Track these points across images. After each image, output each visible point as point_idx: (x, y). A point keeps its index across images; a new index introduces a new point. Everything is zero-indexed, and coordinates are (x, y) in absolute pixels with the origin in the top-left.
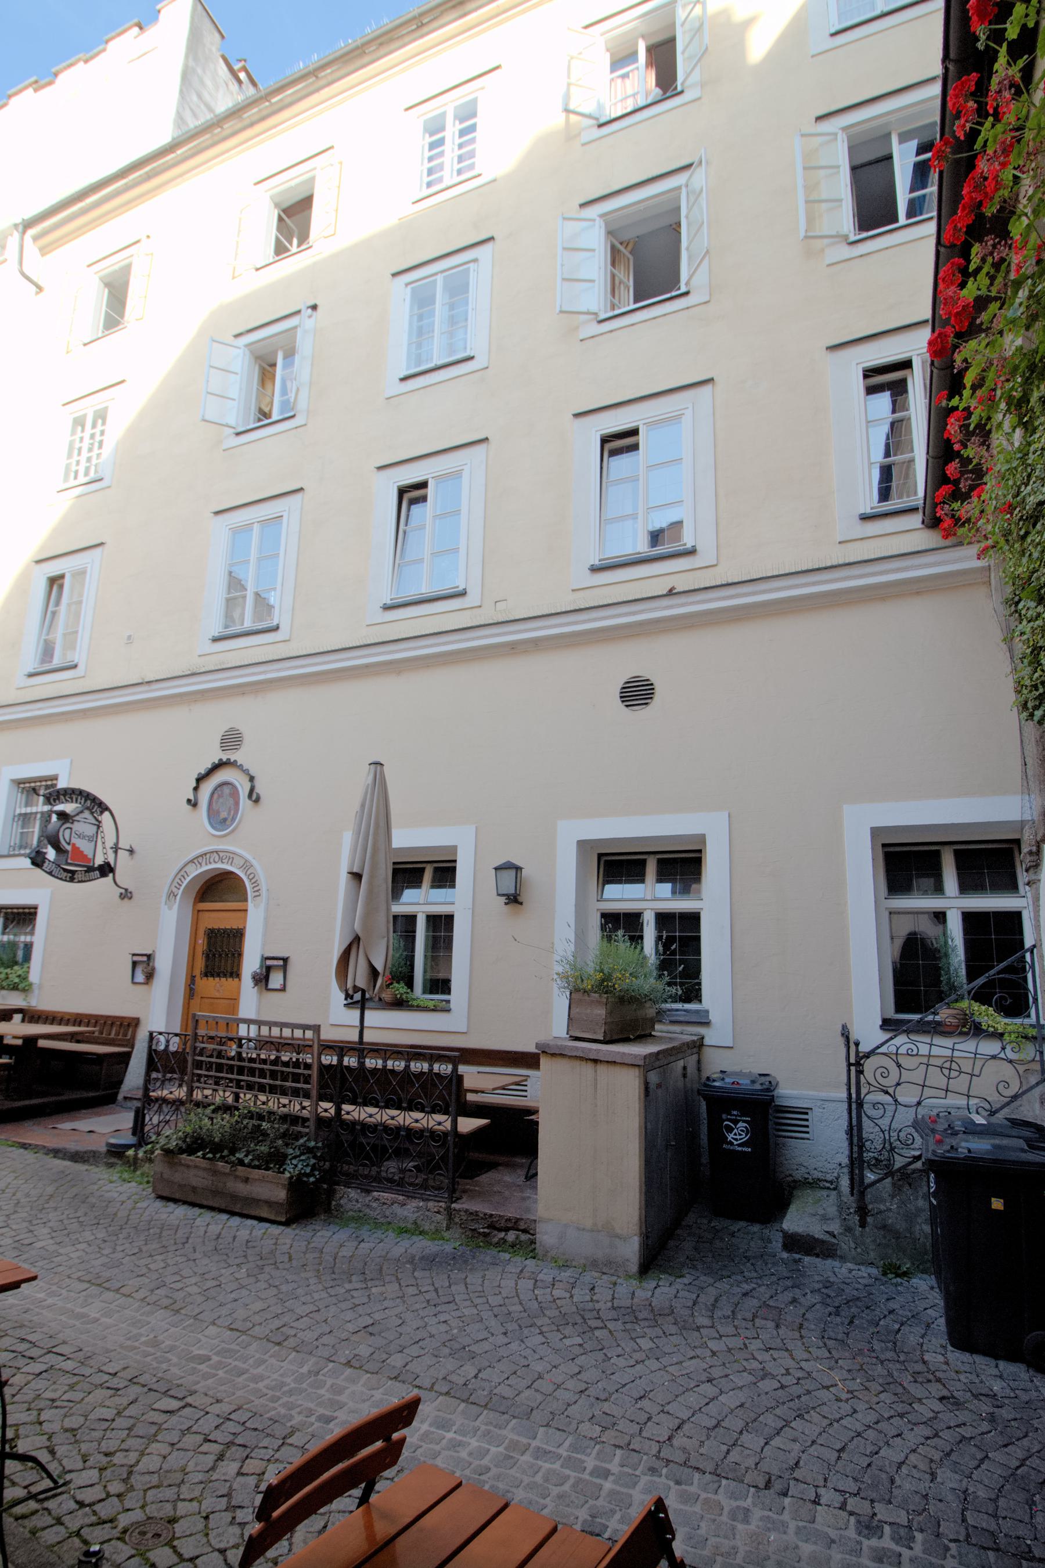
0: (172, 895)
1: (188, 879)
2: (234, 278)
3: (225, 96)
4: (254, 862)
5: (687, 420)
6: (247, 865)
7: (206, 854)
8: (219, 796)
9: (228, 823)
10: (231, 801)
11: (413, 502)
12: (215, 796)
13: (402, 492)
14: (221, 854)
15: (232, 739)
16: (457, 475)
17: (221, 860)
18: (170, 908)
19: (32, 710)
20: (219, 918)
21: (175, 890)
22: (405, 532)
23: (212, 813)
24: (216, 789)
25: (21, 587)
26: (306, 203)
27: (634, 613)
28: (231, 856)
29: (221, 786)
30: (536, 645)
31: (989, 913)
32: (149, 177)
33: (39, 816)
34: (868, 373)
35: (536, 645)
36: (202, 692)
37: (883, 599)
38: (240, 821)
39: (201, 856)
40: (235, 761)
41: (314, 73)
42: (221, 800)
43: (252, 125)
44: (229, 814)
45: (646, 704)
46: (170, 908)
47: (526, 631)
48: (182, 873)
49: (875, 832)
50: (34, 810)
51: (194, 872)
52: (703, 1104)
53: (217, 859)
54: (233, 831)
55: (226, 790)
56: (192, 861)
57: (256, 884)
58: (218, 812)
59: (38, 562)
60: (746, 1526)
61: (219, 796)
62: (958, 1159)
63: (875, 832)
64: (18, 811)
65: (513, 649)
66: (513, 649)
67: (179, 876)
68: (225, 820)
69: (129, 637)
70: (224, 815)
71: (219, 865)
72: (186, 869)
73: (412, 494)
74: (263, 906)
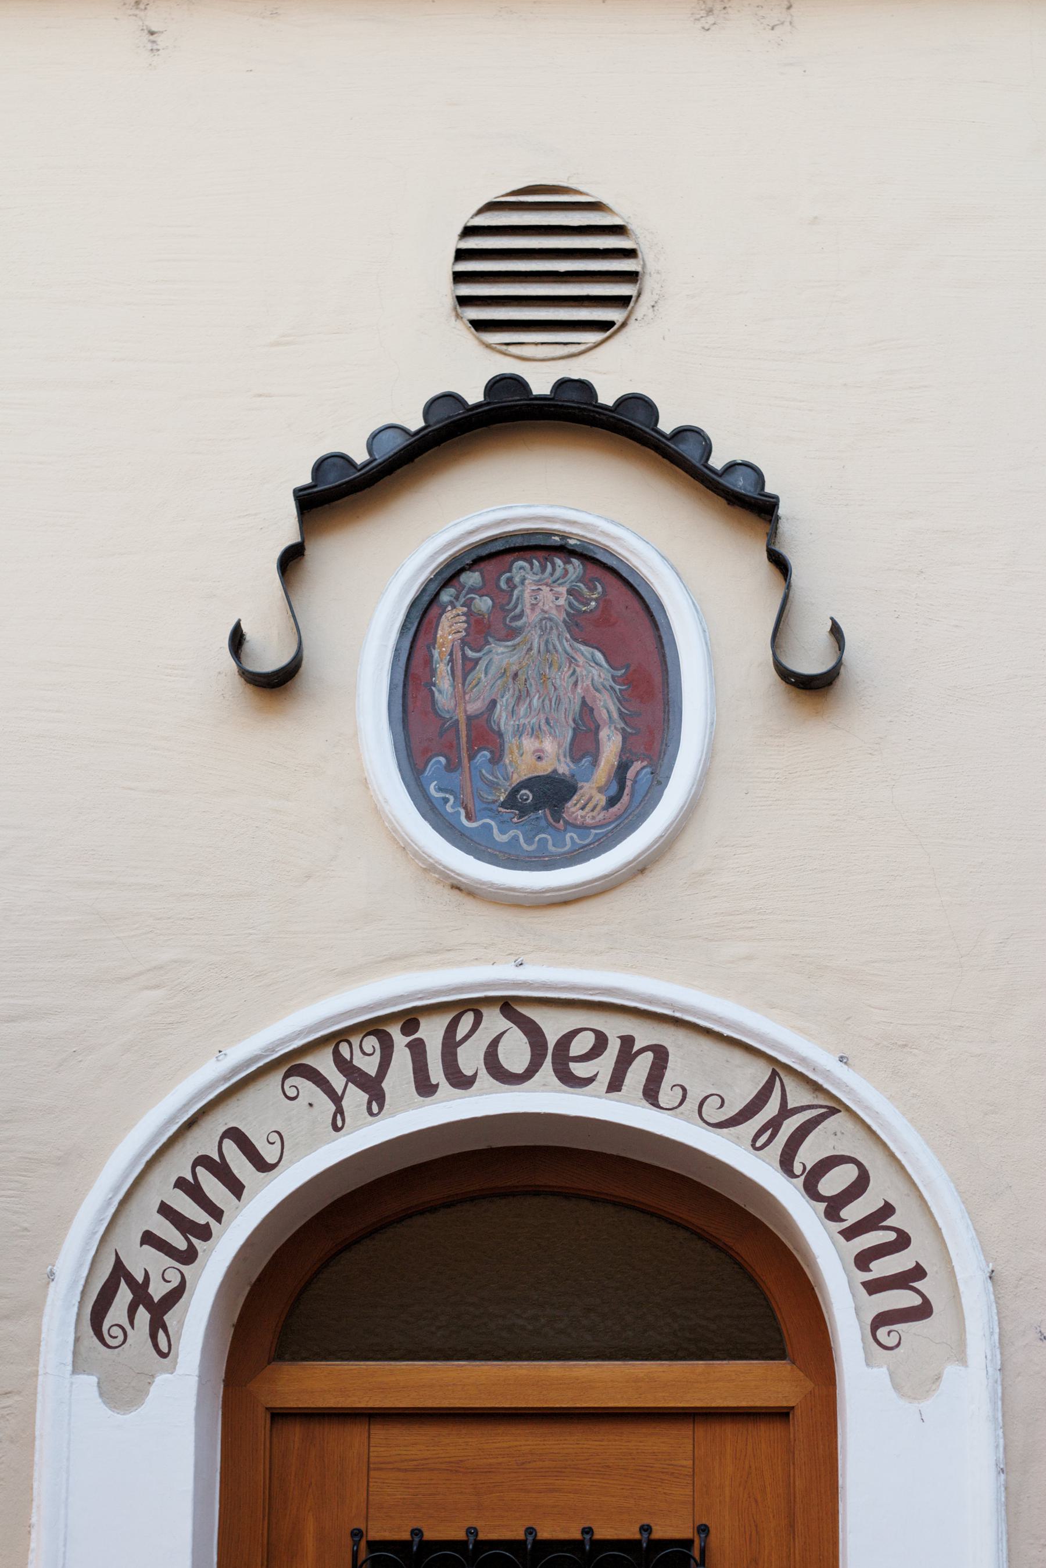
0: (124, 1302)
1: (266, 1196)
4: (853, 1084)
6: (788, 1102)
7: (410, 1020)
8: (480, 631)
10: (593, 671)
12: (450, 628)
14: (554, 1026)
15: (546, 258)
18: (122, 1394)
21: (143, 1262)
23: (433, 738)
24: (449, 575)
28: (643, 1042)
39: (374, 1028)
42: (500, 655)
45: (604, 326)
46: (122, 1394)
48: (205, 1141)
50: (504, 699)
51: (314, 1147)
52: (581, 585)
53: (515, 1053)
54: (639, 869)
55: (542, 594)
56: (293, 1064)
57: (880, 1237)
58: (484, 736)
60: (510, 733)
61: (480, 631)
62: (380, 464)
67: (180, 1164)
68: (550, 794)
71: (544, 1098)
74: (968, 1388)
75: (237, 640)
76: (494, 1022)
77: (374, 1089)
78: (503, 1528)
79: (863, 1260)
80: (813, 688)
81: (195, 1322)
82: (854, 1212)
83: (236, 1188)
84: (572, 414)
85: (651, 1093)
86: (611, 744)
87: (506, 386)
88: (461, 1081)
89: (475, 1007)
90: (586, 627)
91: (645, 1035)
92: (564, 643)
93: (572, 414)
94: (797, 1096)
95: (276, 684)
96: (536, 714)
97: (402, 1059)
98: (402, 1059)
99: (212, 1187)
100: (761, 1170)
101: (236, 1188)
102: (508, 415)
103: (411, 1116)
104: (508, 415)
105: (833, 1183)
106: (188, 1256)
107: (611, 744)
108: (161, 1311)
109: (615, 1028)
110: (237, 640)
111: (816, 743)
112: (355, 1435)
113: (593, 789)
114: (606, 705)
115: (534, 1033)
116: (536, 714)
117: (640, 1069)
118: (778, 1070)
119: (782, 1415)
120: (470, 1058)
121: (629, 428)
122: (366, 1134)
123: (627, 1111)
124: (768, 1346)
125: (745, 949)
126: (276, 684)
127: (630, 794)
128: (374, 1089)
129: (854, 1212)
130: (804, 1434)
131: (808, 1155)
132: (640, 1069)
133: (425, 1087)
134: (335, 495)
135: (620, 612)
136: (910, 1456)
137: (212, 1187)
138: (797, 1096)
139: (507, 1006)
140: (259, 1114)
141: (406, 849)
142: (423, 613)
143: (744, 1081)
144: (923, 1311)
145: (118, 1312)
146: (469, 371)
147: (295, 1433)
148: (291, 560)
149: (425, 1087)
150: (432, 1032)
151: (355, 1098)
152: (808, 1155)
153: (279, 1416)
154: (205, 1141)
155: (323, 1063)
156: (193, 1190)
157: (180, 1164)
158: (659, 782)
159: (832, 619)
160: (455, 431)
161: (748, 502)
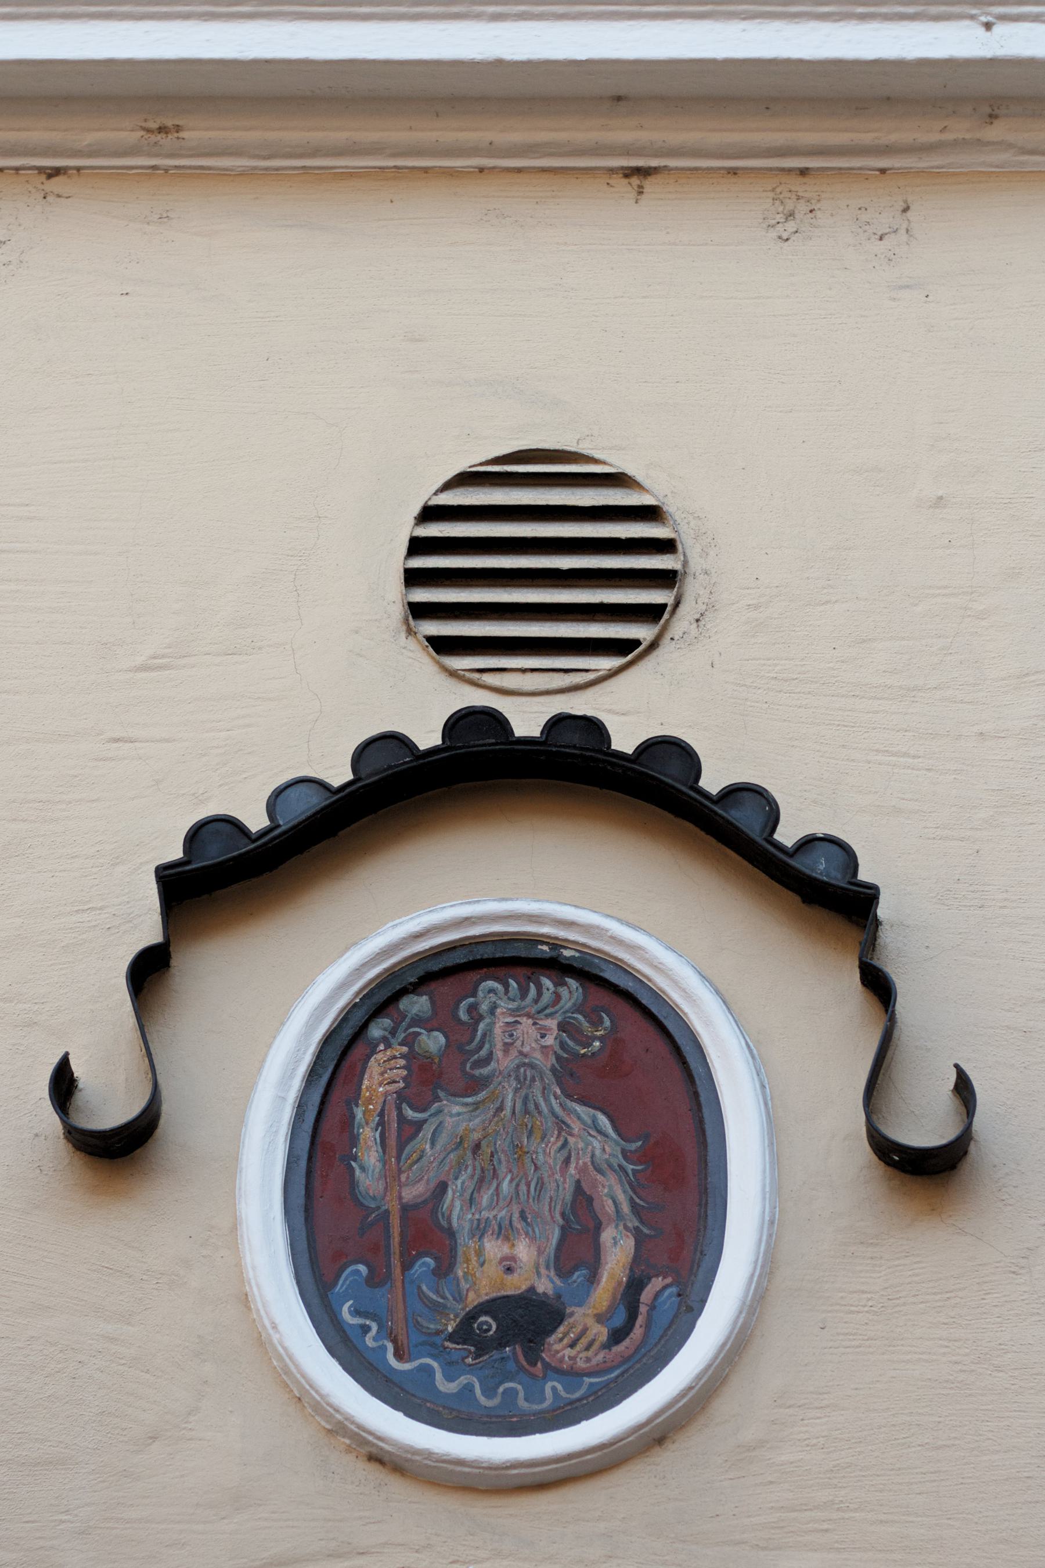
8: (425, 1081)
10: (594, 1141)
12: (380, 1076)
15: (541, 552)
23: (342, 1235)
40: (671, 754)
42: (455, 1115)
44: (577, 1251)
55: (521, 1028)
58: (427, 1234)
61: (425, 1081)
68: (525, 1322)
70: (506, 1261)
75: (63, 1084)
86: (617, 1252)
87: (473, 726)
90: (585, 1077)
92: (551, 1100)
95: (118, 1150)
107: (617, 1252)
110: (63, 1084)
113: (588, 1316)
114: (612, 1193)
126: (118, 1150)
127: (644, 1333)
134: (221, 878)
135: (637, 1058)
141: (304, 1400)
142: (341, 1054)
146: (423, 707)
148: (148, 972)
159: (67, 1054)
160: (395, 793)
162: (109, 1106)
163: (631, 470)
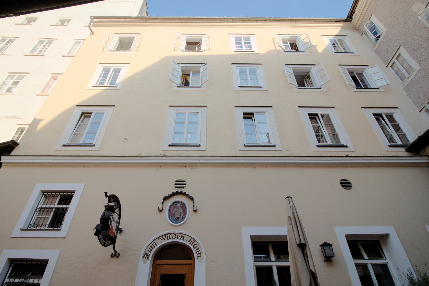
0: (146, 255)
1: (157, 247)
2: (103, 51)
3: (145, 15)
5: (200, 114)
6: (192, 240)
7: (167, 234)
8: (174, 207)
9: (180, 219)
10: (181, 210)
11: (85, 117)
12: (172, 207)
13: (83, 114)
14: (177, 235)
15: (180, 183)
16: (103, 113)
17: (177, 237)
18: (145, 263)
19: (67, 160)
20: (173, 267)
21: (148, 253)
22: (80, 125)
23: (171, 215)
24: (173, 204)
25: (67, 113)
26: (50, 42)
27: (340, 160)
29: (177, 203)
30: (307, 165)
31: (263, 267)
32: (144, 22)
33: (54, 210)
34: (244, 114)
35: (307, 165)
36: (154, 164)
37: (405, 167)
38: (187, 220)
39: (165, 235)
40: (185, 193)
41: (179, 19)
42: (176, 209)
43: (181, 22)
44: (180, 215)
46: (145, 263)
47: (306, 160)
48: (153, 243)
49: (252, 237)
50: (52, 206)
51: (160, 243)
53: (174, 237)
54: (183, 224)
55: (179, 205)
56: (159, 238)
57: (198, 250)
58: (174, 214)
59: (77, 106)
61: (174, 207)
63: (252, 237)
64: (40, 206)
65: (298, 165)
66: (298, 165)
67: (151, 245)
68: (178, 218)
69: (126, 139)
70: (177, 216)
71: (176, 240)
72: (156, 241)
73: (86, 115)
74: (203, 262)
75: (159, 208)
76: (173, 234)
77: (164, 239)
78: (171, 273)
79: (197, 252)
80: (195, 211)
81: (150, 257)
82: (196, 249)
83: (154, 247)
84: (181, 193)
85: (183, 240)
86: (182, 215)
87: (177, 191)
88: (170, 239)
89: (172, 233)
90: (181, 207)
91: (183, 235)
92: (180, 208)
93: (181, 193)
94: (193, 240)
95: (161, 211)
96: (177, 214)
97: (167, 237)
98: (167, 237)
99: (153, 247)
100: (190, 245)
101: (154, 247)
102: (177, 193)
103: (167, 241)
104: (177, 193)
105: (195, 246)
106: (151, 252)
107: (182, 215)
108: (148, 256)
109: (181, 235)
110: (159, 208)
111: (196, 214)
112: (162, 266)
113: (181, 218)
114: (182, 212)
115: (176, 235)
116: (177, 214)
117: (182, 238)
118: (192, 238)
119: (191, 264)
120: (171, 237)
121: (184, 194)
122: (164, 243)
123: (181, 241)
124: (191, 259)
125: (190, 231)
126: (161, 211)
127: (183, 218)
128: (164, 239)
129: (196, 249)
130: (192, 265)
131: (193, 244)
132: (182, 238)
133: (168, 239)
134: (166, 198)
135: (183, 206)
136: (200, 268)
137: (153, 247)
138: (193, 240)
139: (174, 233)
140: (156, 241)
141: (168, 222)
142: (171, 206)
143: (190, 238)
144: (201, 256)
145: (145, 256)
146: (175, 190)
147: (157, 266)
148: (163, 203)
149: (168, 239)
150: (169, 235)
151: (163, 240)
152: (193, 244)
153: (157, 264)
154: (153, 243)
155: (161, 238)
156: (151, 247)
157: (151, 245)
158: (184, 219)
159: (37, 18)
160: (174, 194)
161: (192, 199)
162: (160, 209)
163: (389, 147)
